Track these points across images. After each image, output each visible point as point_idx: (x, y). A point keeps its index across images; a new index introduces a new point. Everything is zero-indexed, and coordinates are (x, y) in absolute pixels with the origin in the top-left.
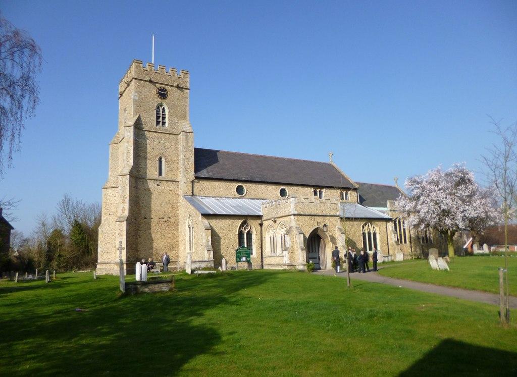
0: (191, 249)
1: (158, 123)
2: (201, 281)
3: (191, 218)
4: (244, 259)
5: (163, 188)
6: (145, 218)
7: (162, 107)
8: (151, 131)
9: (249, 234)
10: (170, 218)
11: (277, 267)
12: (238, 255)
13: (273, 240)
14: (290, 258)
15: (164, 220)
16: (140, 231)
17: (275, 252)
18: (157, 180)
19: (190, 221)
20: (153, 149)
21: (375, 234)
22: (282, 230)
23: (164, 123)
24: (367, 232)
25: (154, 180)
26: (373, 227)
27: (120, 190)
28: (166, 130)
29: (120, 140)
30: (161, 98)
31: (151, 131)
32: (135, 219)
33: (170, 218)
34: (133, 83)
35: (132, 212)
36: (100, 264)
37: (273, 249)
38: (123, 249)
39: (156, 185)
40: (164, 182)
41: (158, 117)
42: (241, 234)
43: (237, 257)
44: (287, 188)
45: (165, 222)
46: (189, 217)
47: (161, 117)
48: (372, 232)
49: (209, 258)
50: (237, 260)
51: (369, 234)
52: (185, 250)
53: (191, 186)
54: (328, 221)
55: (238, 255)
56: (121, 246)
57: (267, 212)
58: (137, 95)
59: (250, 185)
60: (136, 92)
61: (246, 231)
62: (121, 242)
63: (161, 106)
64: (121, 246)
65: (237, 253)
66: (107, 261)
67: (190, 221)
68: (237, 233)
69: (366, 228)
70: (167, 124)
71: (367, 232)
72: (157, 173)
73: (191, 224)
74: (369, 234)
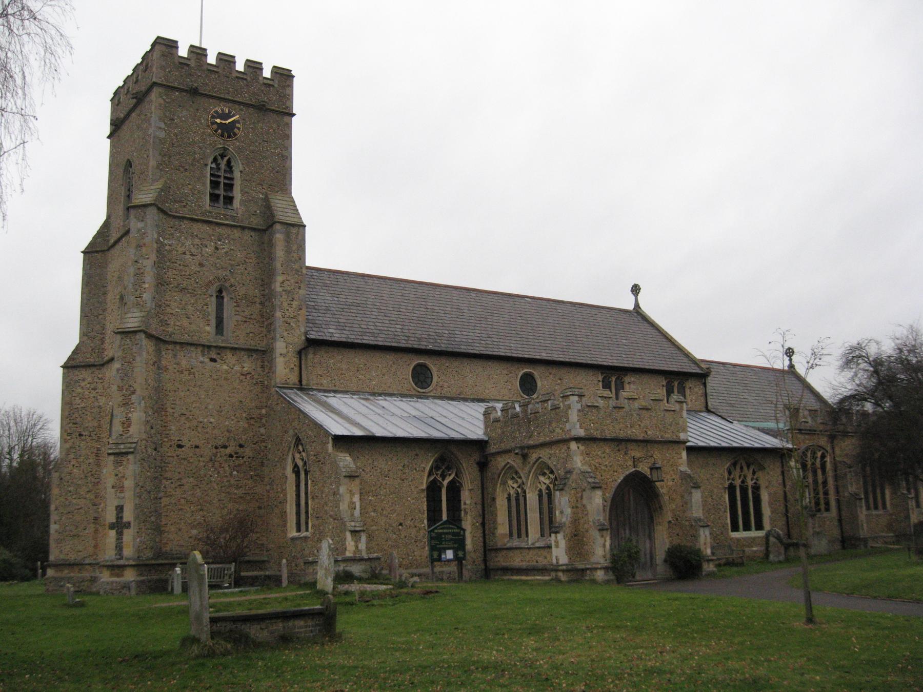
0: (303, 527)
1: (214, 198)
2: (808, 496)
3: (300, 448)
4: (449, 554)
5: (225, 367)
6: (180, 446)
7: (226, 159)
8: (197, 221)
9: (455, 490)
10: (241, 446)
11: (527, 575)
12: (434, 543)
13: (518, 504)
14: (570, 550)
15: (228, 451)
16: (166, 479)
17: (524, 535)
18: (209, 347)
19: (297, 456)
20: (201, 265)
21: (756, 488)
22: (542, 478)
23: (229, 200)
24: (738, 482)
25: (203, 346)
26: (751, 471)
27: (118, 370)
28: (234, 218)
29: (112, 241)
30: (222, 135)
31: (197, 221)
32: (155, 449)
33: (241, 446)
34: (154, 95)
35: (148, 428)
36: (58, 566)
37: (519, 527)
38: (128, 525)
39: (207, 360)
40: (229, 354)
41: (215, 184)
42: (433, 490)
43: (432, 549)
44: (537, 372)
45: (231, 456)
46: (297, 445)
47: (222, 183)
48: (750, 483)
49: (355, 552)
50: (432, 556)
51: (744, 490)
52: (285, 532)
53: (297, 364)
54: (659, 456)
55: (434, 543)
56: (119, 517)
57: (500, 431)
58: (163, 126)
59: (445, 362)
60: (160, 119)
61: (445, 483)
62: (120, 509)
63: (223, 156)
64: (119, 517)
65: (432, 538)
66: (72, 557)
67: (297, 456)
68: (424, 486)
69: (736, 473)
70: (236, 203)
71: (738, 482)
72: (211, 329)
73: (300, 464)
74: (744, 490)
